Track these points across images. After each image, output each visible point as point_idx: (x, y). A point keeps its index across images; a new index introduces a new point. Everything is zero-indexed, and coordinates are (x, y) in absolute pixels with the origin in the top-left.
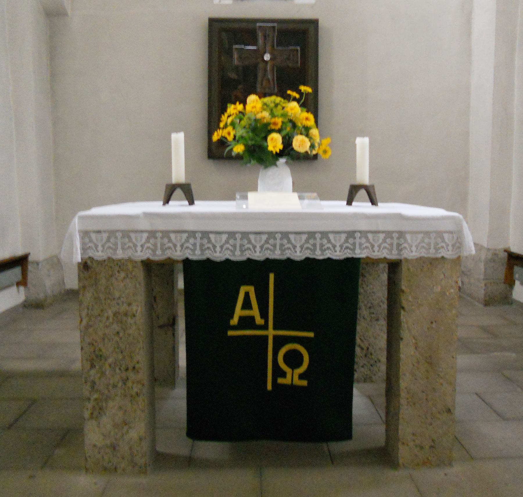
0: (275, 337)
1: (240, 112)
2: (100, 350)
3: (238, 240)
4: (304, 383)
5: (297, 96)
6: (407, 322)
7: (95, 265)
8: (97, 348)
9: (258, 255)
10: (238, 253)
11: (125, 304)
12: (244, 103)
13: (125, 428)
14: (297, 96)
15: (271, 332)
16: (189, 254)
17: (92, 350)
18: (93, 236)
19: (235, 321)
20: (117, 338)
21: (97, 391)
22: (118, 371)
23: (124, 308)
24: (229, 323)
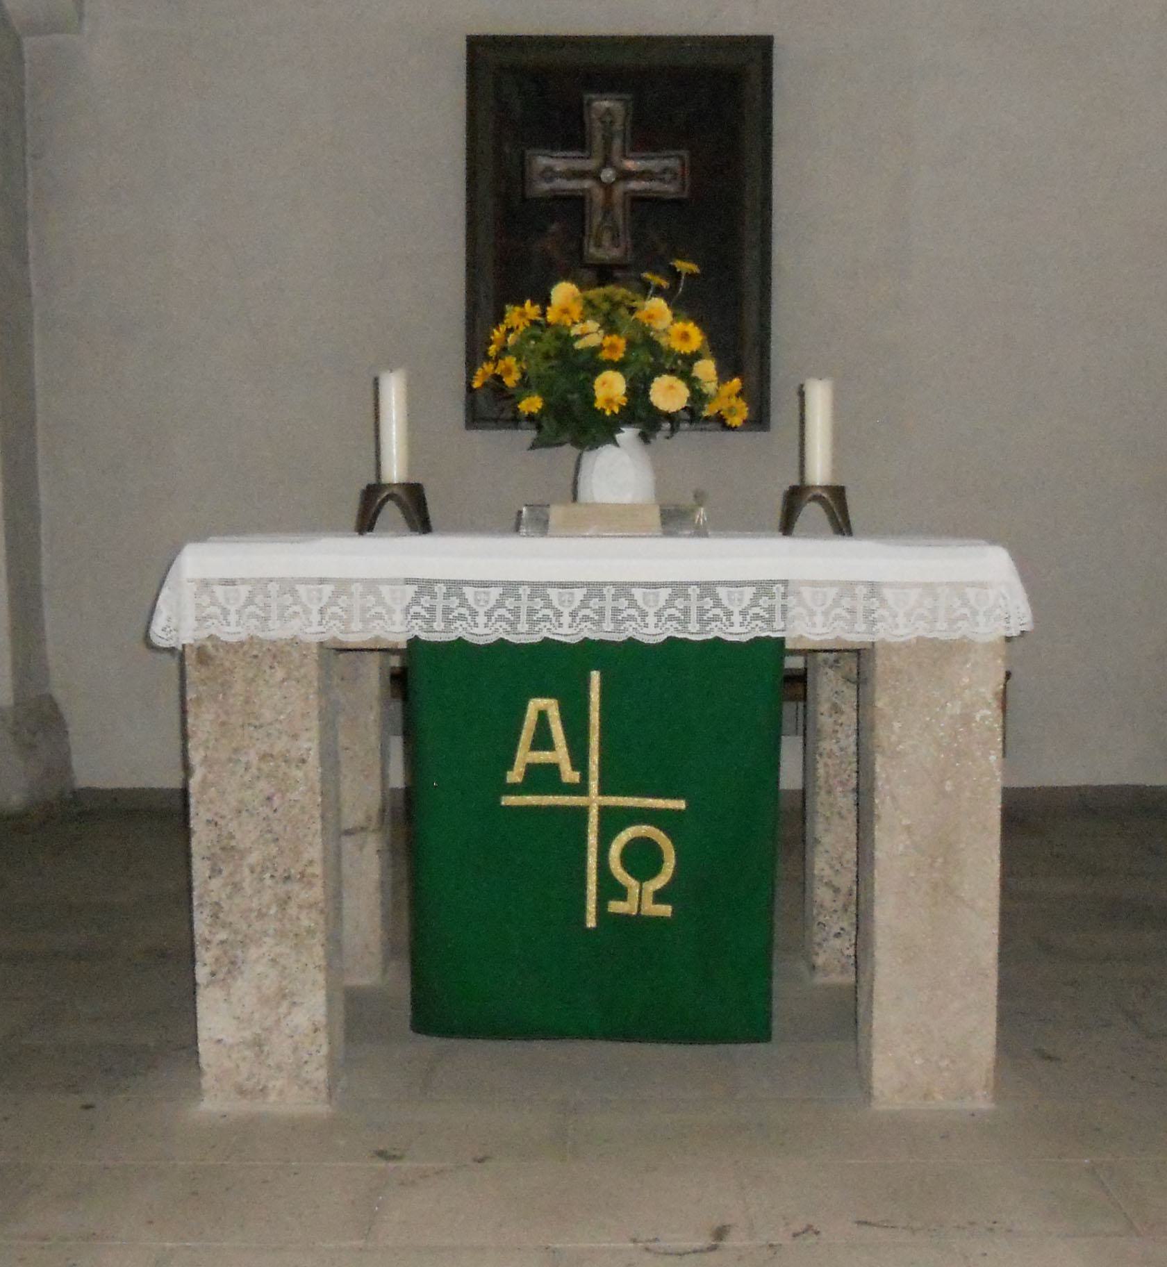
0: (603, 810)
1: (534, 323)
2: (232, 837)
3: (440, 597)
4: (665, 910)
5: (665, 284)
6: (888, 780)
7: (222, 653)
8: (225, 834)
9: (567, 632)
10: (523, 627)
11: (285, 738)
12: (545, 301)
13: (285, 1005)
14: (665, 284)
15: (594, 801)
16: (421, 628)
17: (213, 836)
18: (219, 591)
19: (515, 776)
20: (265, 811)
21: (224, 926)
22: (268, 882)
23: (280, 745)
24: (504, 778)
